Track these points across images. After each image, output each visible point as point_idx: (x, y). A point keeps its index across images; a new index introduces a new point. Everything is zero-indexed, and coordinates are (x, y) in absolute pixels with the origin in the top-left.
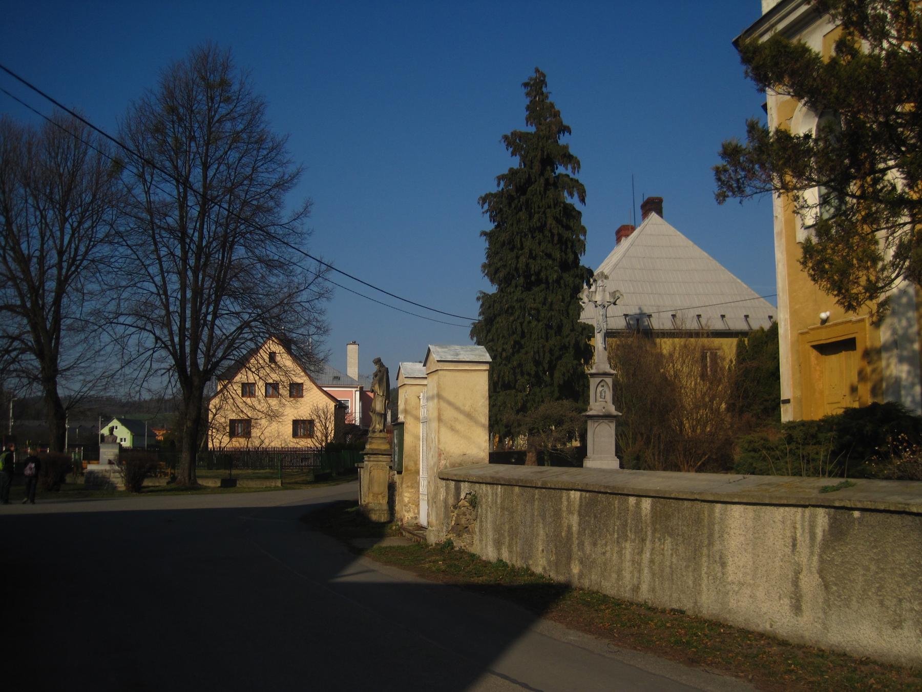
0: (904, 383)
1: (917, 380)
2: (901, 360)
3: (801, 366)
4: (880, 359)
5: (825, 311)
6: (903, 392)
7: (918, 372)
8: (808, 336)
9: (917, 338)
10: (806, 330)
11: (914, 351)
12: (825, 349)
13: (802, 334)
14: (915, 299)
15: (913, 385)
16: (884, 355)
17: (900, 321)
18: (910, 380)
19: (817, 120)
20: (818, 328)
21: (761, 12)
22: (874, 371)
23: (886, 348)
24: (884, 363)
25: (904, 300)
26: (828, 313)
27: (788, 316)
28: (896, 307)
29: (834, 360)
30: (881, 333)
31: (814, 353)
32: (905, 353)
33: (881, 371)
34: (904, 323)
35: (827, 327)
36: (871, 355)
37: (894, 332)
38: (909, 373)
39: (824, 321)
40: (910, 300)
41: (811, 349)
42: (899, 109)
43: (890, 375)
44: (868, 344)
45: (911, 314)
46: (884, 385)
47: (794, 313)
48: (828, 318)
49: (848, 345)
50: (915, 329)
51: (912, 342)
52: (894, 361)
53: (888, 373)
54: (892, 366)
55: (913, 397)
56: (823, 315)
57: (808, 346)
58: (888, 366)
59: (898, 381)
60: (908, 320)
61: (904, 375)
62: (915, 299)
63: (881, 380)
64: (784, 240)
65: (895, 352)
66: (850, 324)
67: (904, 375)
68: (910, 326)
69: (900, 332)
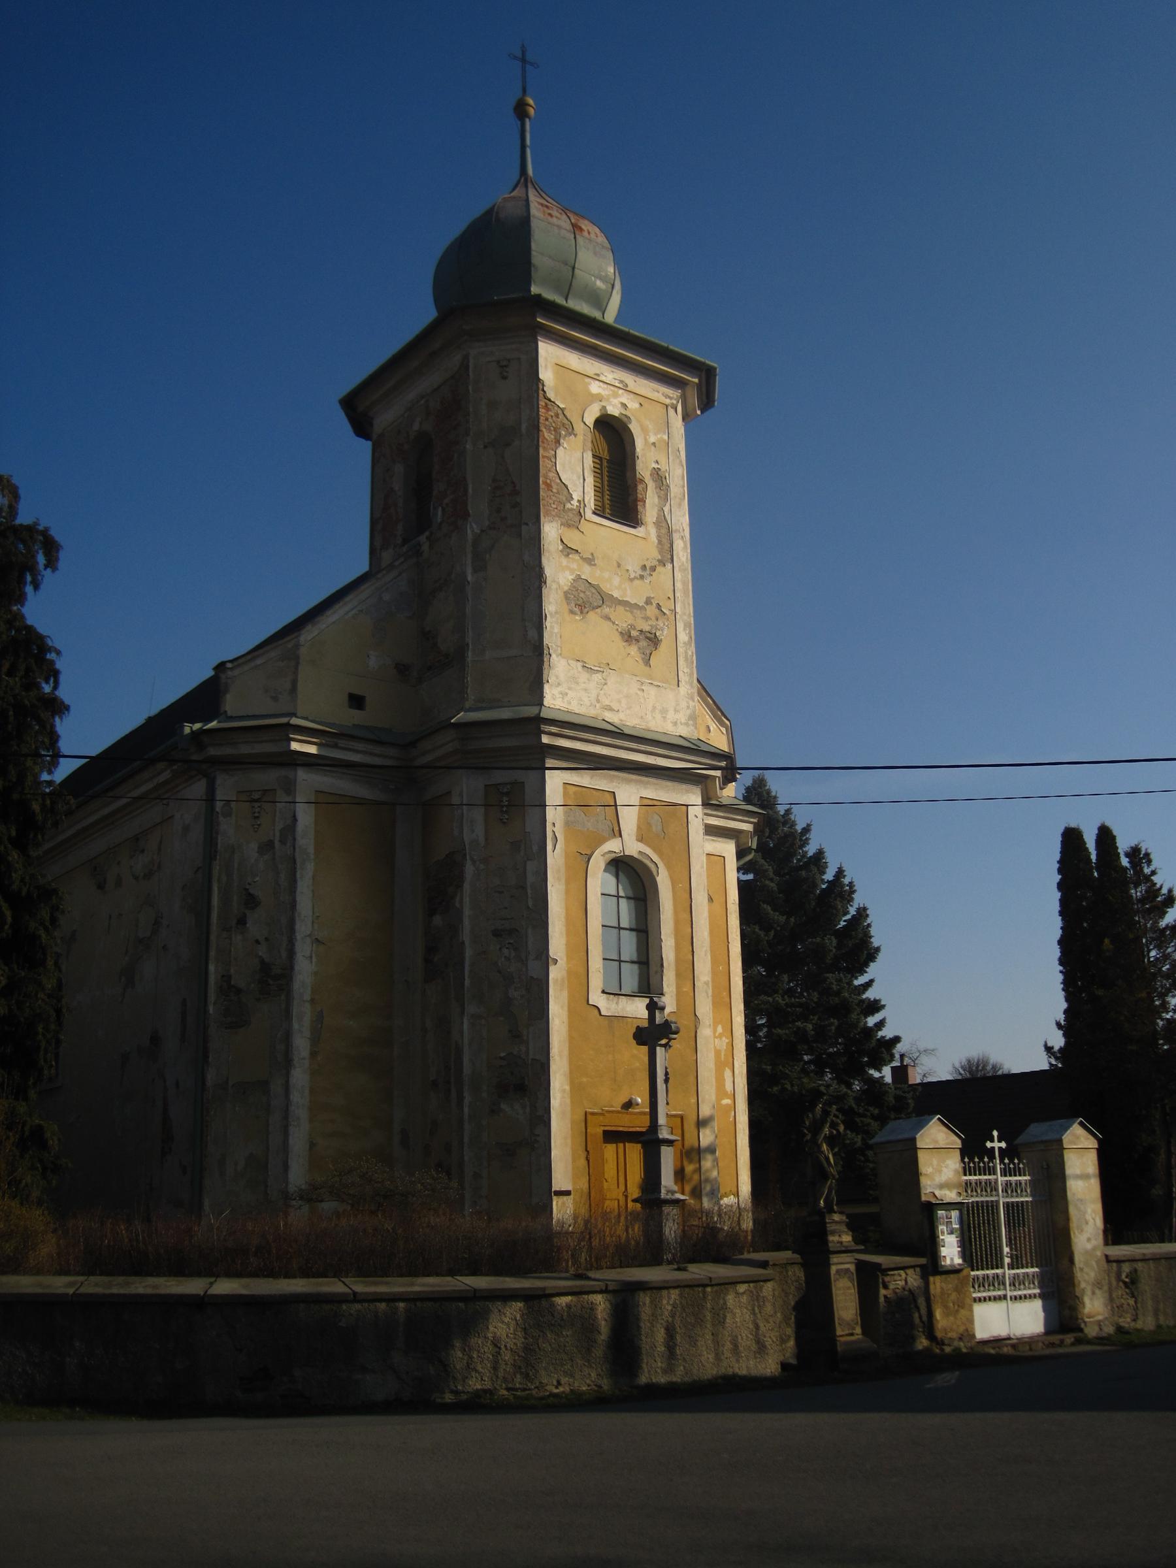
8: (601, 1118)
47: (577, 1089)
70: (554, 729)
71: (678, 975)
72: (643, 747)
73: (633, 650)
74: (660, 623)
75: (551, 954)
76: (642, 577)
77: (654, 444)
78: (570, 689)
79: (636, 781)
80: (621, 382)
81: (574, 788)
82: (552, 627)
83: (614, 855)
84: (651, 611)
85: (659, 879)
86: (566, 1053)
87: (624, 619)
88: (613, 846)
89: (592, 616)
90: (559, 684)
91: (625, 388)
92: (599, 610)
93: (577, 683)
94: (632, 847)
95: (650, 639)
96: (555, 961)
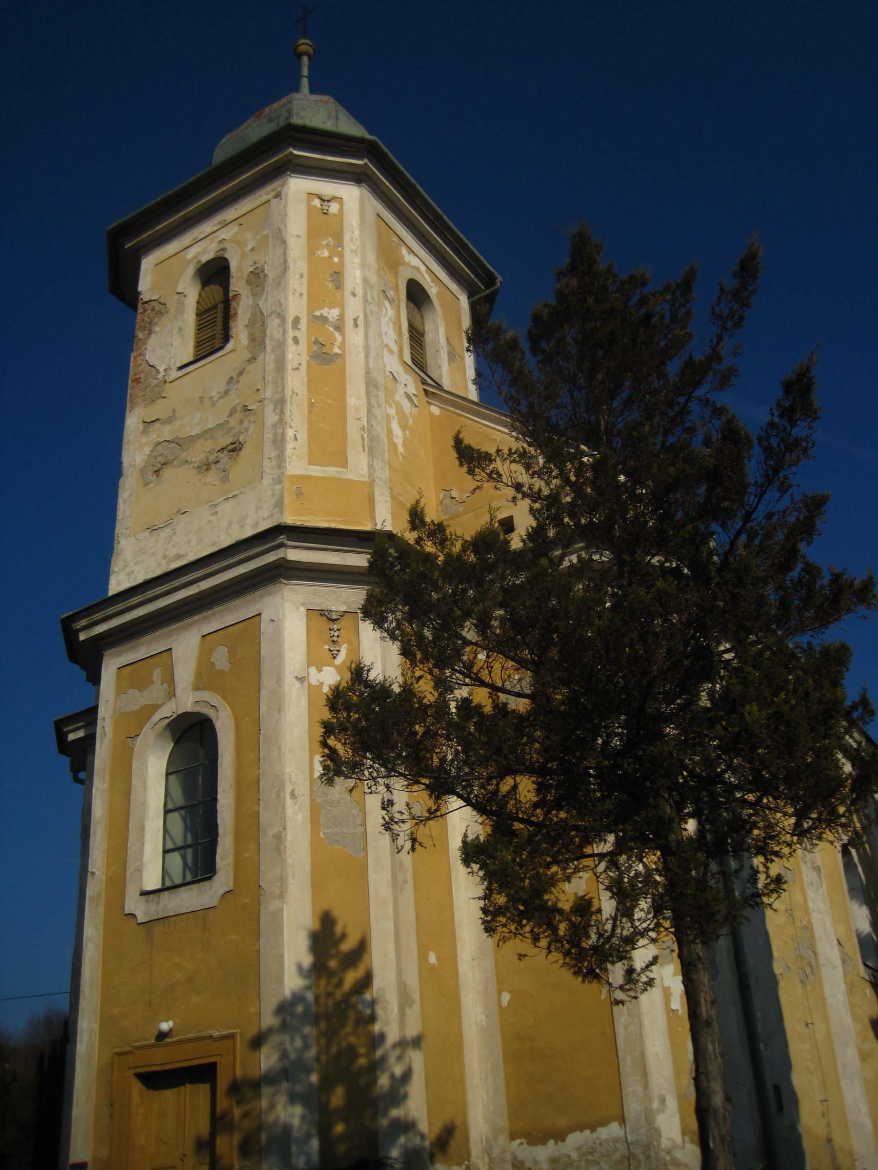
0: (295, 1134)
1: (313, 1130)
2: (293, 1098)
3: (114, 1107)
4: (258, 1096)
5: (167, 1021)
6: (294, 1149)
7: (316, 1117)
8: (131, 1058)
9: (316, 1065)
10: (127, 1049)
11: (310, 1085)
12: (154, 1080)
13: (119, 1054)
14: (313, 1008)
15: (308, 1137)
16: (266, 1091)
17: (292, 1040)
18: (305, 1128)
19: (172, 744)
20: (151, 1046)
21: (107, 593)
22: (246, 1115)
23: (270, 1079)
24: (264, 1103)
25: (300, 1009)
26: (171, 1023)
27: (96, 1026)
28: (288, 1018)
29: (169, 1096)
30: (262, 1057)
31: (137, 1086)
32: (299, 1088)
33: (260, 1114)
34: (298, 1043)
35: (167, 1045)
36: (246, 1089)
37: (284, 1055)
38: (303, 1118)
39: (162, 1036)
40: (307, 1008)
41: (134, 1078)
42: (855, 817)
43: (275, 1122)
44: (239, 1073)
45: (308, 1030)
46: (264, 1137)
47: (107, 1022)
48: (171, 1030)
49: (205, 1073)
50: (313, 1052)
51: (308, 1071)
52: (282, 1099)
53: (271, 1118)
54: (279, 1108)
55: (308, 1155)
56: (165, 1026)
57: (129, 1075)
58: (272, 1106)
59: (287, 1129)
60: (304, 1038)
61: (296, 1122)
62: (313, 1008)
63: (259, 1129)
64: (102, 908)
65: (285, 1085)
66: (209, 1041)
67: (296, 1122)
68: (306, 1047)
69: (292, 1056)
70: (83, 622)
71: (239, 838)
72: (176, 583)
73: (212, 477)
74: (246, 424)
75: (90, 870)
76: (226, 392)
77: (253, 249)
78: (137, 564)
79: (196, 622)
80: (220, 223)
81: (128, 669)
82: (124, 514)
83: (167, 721)
84: (239, 415)
85: (218, 725)
86: (99, 980)
87: (198, 453)
88: (169, 710)
89: (168, 473)
90: (126, 566)
91: (225, 225)
92: (175, 462)
93: (145, 553)
94: (187, 701)
95: (233, 451)
96: (93, 873)
